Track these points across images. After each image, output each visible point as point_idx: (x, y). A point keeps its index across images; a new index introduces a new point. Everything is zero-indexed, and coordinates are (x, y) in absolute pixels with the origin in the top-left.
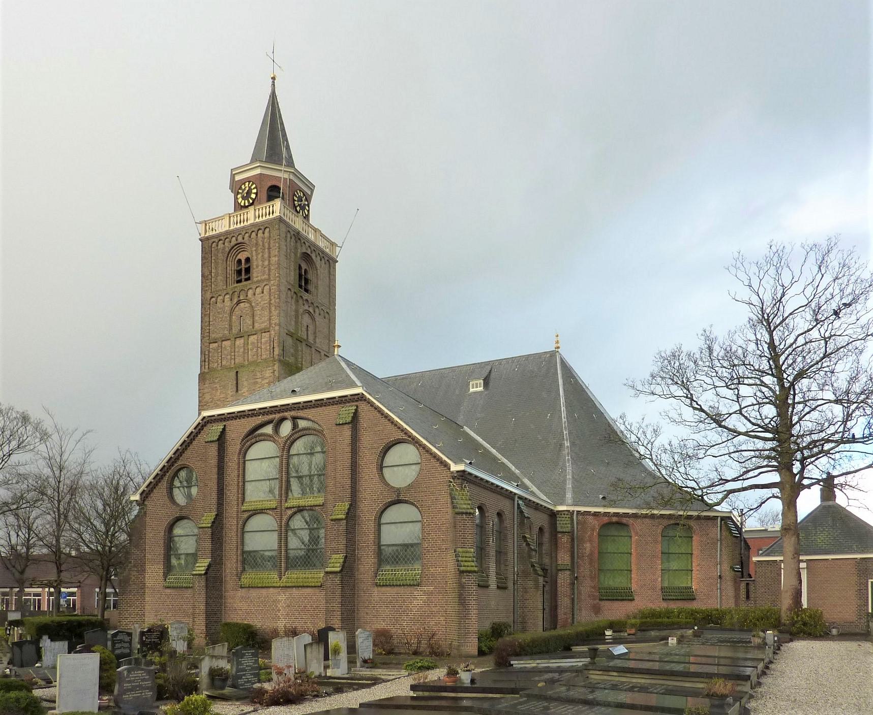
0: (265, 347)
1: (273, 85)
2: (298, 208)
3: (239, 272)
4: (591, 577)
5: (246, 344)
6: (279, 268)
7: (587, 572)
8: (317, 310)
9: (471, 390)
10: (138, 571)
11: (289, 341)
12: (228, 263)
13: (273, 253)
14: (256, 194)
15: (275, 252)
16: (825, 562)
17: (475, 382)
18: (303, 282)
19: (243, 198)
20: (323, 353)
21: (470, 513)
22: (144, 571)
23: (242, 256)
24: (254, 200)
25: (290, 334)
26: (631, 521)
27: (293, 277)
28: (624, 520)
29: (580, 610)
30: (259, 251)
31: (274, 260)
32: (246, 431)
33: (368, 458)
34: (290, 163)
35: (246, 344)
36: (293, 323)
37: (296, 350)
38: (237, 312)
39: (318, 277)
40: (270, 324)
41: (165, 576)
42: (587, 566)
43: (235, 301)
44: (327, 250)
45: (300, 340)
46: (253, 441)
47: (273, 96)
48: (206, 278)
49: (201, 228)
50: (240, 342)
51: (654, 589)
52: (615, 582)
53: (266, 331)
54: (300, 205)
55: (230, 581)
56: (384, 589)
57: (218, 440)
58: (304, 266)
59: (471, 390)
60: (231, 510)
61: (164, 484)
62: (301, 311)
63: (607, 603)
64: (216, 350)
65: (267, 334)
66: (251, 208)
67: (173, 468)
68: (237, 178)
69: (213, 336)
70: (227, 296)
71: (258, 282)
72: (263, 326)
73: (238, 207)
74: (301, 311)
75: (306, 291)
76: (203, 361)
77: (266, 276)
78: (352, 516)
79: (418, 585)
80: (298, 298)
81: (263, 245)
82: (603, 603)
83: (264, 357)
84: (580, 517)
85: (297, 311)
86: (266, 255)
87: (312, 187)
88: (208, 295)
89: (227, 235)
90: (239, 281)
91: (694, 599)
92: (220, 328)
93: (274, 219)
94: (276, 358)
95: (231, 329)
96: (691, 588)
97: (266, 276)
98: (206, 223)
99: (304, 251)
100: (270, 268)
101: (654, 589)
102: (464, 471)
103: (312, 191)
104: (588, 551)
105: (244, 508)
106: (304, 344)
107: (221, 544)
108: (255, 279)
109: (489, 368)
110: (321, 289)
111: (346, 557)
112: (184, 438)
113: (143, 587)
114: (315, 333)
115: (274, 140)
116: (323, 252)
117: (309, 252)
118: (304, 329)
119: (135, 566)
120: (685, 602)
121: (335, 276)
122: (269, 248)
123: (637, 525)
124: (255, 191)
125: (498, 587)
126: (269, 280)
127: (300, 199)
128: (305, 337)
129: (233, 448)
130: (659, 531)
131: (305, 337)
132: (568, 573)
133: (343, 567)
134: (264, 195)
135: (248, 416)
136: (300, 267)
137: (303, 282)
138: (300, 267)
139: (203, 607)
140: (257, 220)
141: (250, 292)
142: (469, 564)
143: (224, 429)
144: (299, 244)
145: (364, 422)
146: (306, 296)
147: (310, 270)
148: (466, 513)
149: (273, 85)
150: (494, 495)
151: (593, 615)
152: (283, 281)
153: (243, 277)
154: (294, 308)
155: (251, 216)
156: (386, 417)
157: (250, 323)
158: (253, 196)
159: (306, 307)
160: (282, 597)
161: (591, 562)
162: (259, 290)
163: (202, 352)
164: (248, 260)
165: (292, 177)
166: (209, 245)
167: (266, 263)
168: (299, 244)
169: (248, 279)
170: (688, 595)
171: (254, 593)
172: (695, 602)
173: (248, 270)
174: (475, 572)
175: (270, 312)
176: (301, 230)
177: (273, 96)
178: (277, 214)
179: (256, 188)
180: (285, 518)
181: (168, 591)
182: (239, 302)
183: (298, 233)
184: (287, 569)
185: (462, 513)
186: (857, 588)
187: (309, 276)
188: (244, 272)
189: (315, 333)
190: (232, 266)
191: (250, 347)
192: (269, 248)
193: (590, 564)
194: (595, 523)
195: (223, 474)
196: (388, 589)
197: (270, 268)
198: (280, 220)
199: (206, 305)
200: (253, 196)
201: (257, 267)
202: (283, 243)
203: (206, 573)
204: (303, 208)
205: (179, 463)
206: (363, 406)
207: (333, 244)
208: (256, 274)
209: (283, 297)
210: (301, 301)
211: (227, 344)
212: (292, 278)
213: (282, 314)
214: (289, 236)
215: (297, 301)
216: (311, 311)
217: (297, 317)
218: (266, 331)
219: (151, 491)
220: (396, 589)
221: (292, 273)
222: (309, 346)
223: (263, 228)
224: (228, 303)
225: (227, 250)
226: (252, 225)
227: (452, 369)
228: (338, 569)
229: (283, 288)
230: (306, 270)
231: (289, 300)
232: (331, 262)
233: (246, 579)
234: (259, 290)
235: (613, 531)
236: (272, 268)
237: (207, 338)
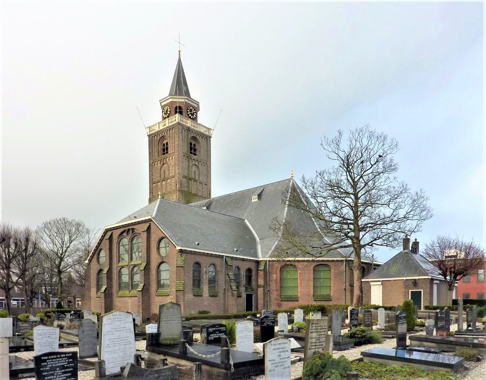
0: (174, 184)
2: (190, 115)
3: (164, 150)
6: (178, 147)
7: (274, 288)
8: (200, 163)
9: (253, 201)
12: (159, 145)
15: (177, 139)
18: (193, 150)
20: (203, 183)
22: (90, 291)
23: (165, 142)
24: (169, 114)
25: (185, 177)
26: (296, 264)
27: (186, 149)
29: (271, 305)
31: (176, 143)
32: (119, 233)
34: (187, 93)
36: (186, 171)
38: (163, 169)
41: (97, 292)
43: (162, 163)
47: (180, 61)
48: (150, 153)
49: (148, 130)
50: (164, 183)
51: (309, 295)
52: (289, 293)
54: (191, 114)
55: (115, 294)
58: (193, 143)
59: (253, 201)
61: (95, 256)
64: (155, 187)
66: (167, 119)
68: (163, 104)
69: (154, 180)
71: (171, 154)
73: (164, 118)
76: (150, 193)
78: (147, 269)
80: (189, 158)
82: (282, 302)
84: (271, 263)
85: (188, 165)
87: (198, 103)
88: (152, 162)
89: (158, 133)
90: (164, 154)
95: (161, 177)
98: (150, 127)
99: (192, 135)
100: (181, 144)
101: (309, 295)
102: (181, 249)
103: (198, 105)
104: (275, 278)
107: (112, 280)
108: (169, 153)
110: (202, 152)
112: (100, 238)
113: (90, 297)
115: (180, 84)
116: (203, 134)
117: (195, 136)
118: (193, 173)
120: (326, 302)
121: (210, 144)
126: (174, 153)
127: (191, 110)
128: (194, 177)
129: (115, 241)
130: (312, 268)
131: (194, 177)
132: (262, 288)
133: (143, 289)
134: (173, 112)
135: (119, 228)
136: (191, 144)
137: (193, 150)
138: (191, 144)
141: (168, 159)
143: (112, 234)
146: (194, 157)
147: (196, 145)
153: (166, 152)
155: (168, 123)
158: (169, 112)
159: (194, 163)
160: (130, 300)
161: (276, 283)
162: (171, 158)
163: (150, 189)
164: (167, 143)
165: (186, 101)
166: (151, 137)
169: (167, 153)
173: (167, 149)
176: (190, 126)
177: (180, 61)
178: (177, 121)
180: (131, 269)
182: (163, 164)
183: (189, 128)
184: (132, 289)
186: (404, 294)
187: (197, 147)
188: (165, 150)
190: (161, 147)
194: (278, 266)
197: (181, 144)
198: (179, 123)
199: (151, 166)
200: (169, 112)
202: (180, 134)
204: (193, 115)
206: (152, 223)
207: (209, 129)
209: (181, 160)
210: (191, 160)
211: (159, 184)
212: (186, 150)
214: (183, 130)
215: (189, 160)
216: (197, 163)
217: (188, 168)
219: (92, 259)
221: (186, 148)
222: (195, 181)
224: (159, 165)
226: (168, 127)
227: (229, 195)
229: (180, 156)
230: (194, 145)
231: (184, 161)
232: (208, 138)
233: (121, 293)
234: (171, 158)
235: (321, 268)
236: (177, 146)
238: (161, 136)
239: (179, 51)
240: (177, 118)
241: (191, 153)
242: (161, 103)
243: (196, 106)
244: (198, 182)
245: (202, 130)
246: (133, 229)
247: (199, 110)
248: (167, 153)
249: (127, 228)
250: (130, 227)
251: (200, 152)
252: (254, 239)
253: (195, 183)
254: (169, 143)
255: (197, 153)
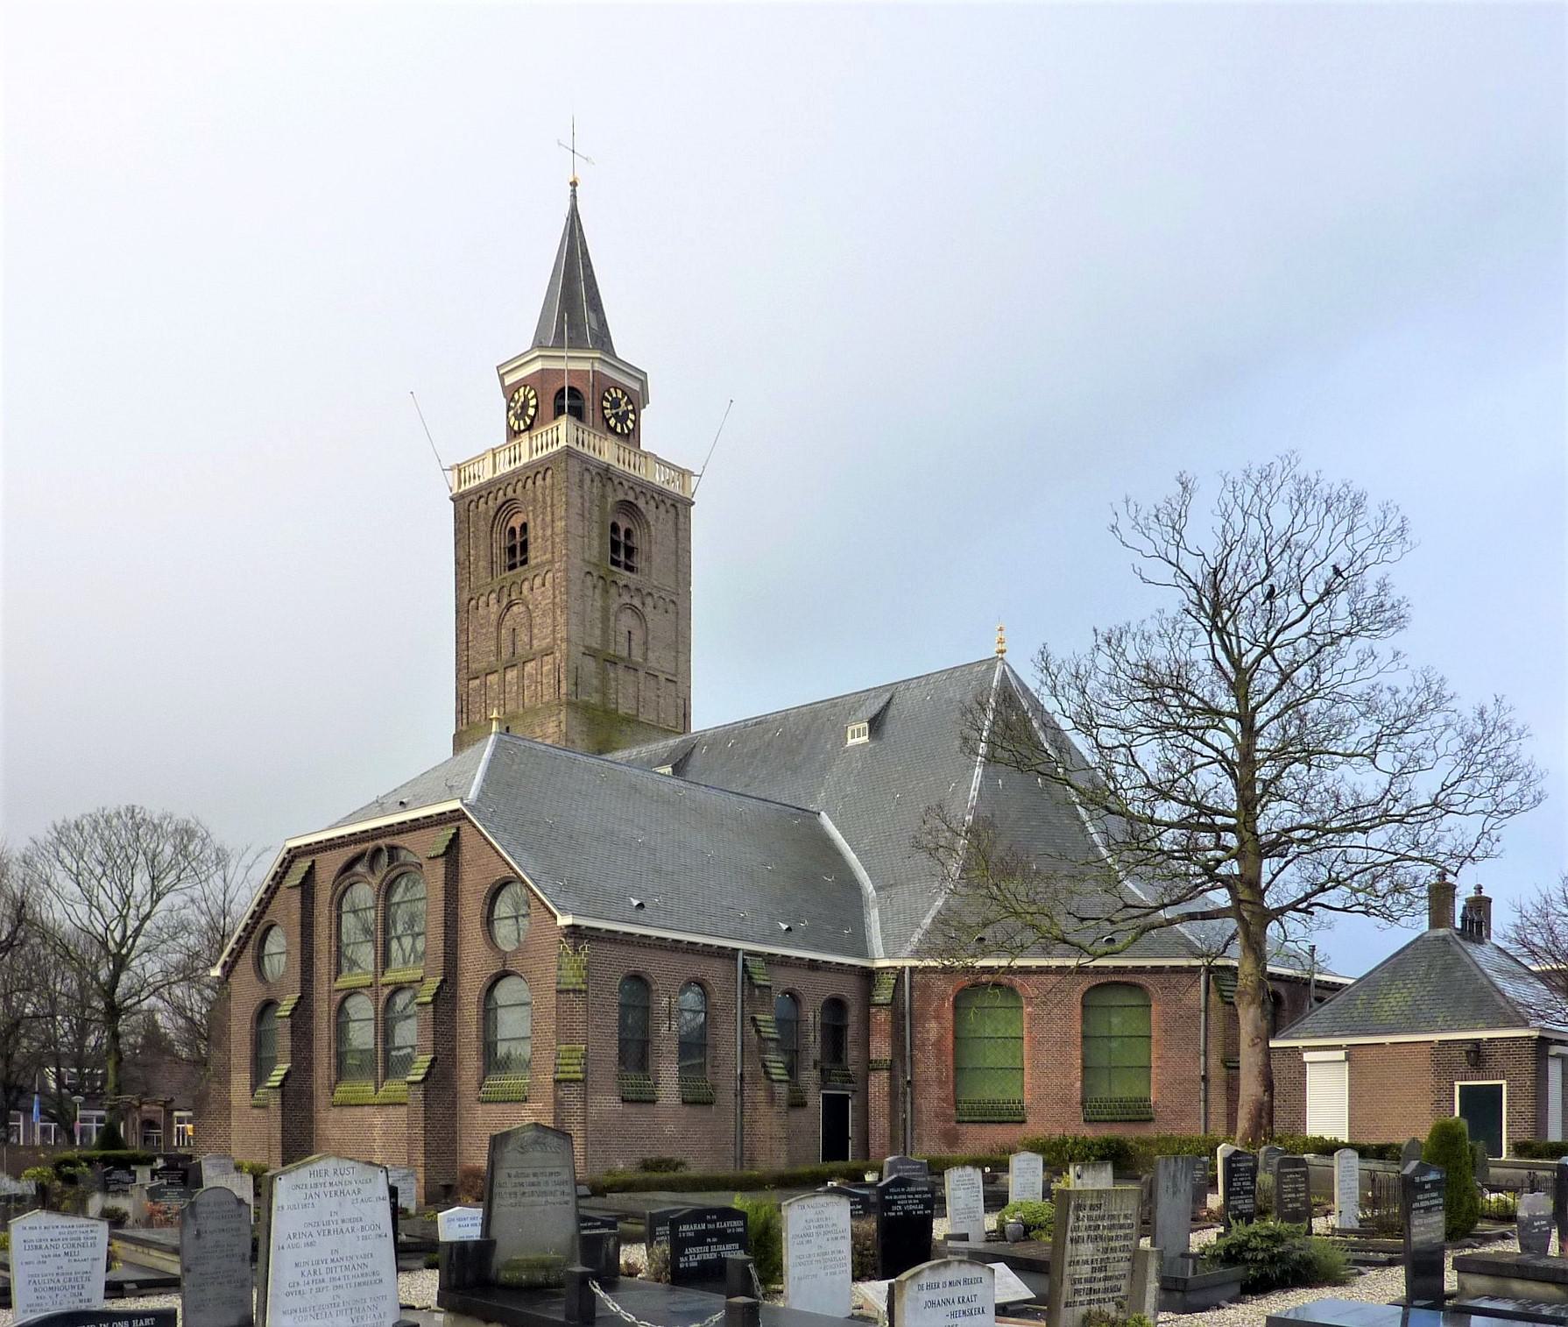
0: (549, 680)
1: (574, 196)
2: (612, 422)
3: (512, 550)
4: (940, 1082)
5: (521, 677)
6: (566, 540)
7: (932, 1073)
8: (649, 601)
9: (851, 742)
10: (219, 1083)
11: (590, 665)
12: (494, 532)
13: (557, 512)
14: (536, 407)
16: (1374, 1051)
17: (856, 727)
19: (517, 417)
20: (662, 677)
21: (580, 991)
22: (229, 1082)
23: (516, 522)
24: (532, 419)
25: (590, 653)
26: (1017, 980)
27: (597, 547)
28: (1004, 980)
30: (539, 511)
31: (560, 524)
33: (471, 909)
34: (603, 340)
35: (521, 677)
36: (598, 632)
37: (604, 681)
39: (652, 540)
40: (554, 639)
42: (933, 1060)
43: (505, 602)
44: (671, 488)
45: (613, 661)
46: (347, 883)
49: (452, 477)
50: (511, 675)
51: (1065, 1101)
52: (989, 1091)
53: (548, 652)
54: (616, 415)
56: (488, 1106)
57: (302, 884)
58: (623, 524)
59: (851, 742)
60: (322, 989)
61: (249, 952)
62: (614, 607)
63: (973, 1129)
65: (549, 659)
67: (259, 926)
68: (509, 380)
70: (493, 596)
71: (537, 566)
72: (544, 643)
73: (513, 434)
74: (614, 607)
75: (630, 568)
76: (459, 712)
77: (548, 556)
78: (446, 997)
79: (526, 1100)
80: (607, 583)
81: (544, 502)
82: (964, 1128)
83: (546, 698)
84: (917, 977)
85: (605, 610)
86: (548, 519)
88: (466, 596)
90: (512, 567)
91: (1151, 1120)
92: (484, 654)
93: (558, 452)
94: (563, 698)
95: (499, 652)
96: (1147, 1100)
97: (548, 556)
98: (459, 468)
99: (621, 497)
100: (577, 535)
102: (573, 926)
104: (933, 1036)
105: (337, 986)
106: (621, 666)
108: (532, 562)
109: (888, 696)
111: (434, 1060)
113: (228, 1106)
114: (646, 643)
115: (575, 301)
116: (661, 492)
117: (631, 498)
118: (622, 640)
119: (215, 1075)
122: (552, 505)
123: (1028, 987)
124: (533, 402)
125: (684, 1102)
126: (552, 562)
127: (616, 403)
129: (324, 894)
131: (625, 654)
133: (428, 1074)
134: (548, 408)
136: (615, 528)
138: (615, 528)
139: (279, 1136)
140: (535, 457)
141: (526, 586)
142: (571, 1068)
143: (312, 867)
144: (609, 489)
145: (467, 853)
146: (624, 576)
147: (635, 533)
148: (574, 991)
149: (574, 196)
150: (676, 955)
151: (944, 1148)
152: (578, 562)
153: (518, 558)
154: (598, 604)
155: (527, 451)
156: (490, 844)
157: (526, 639)
158: (531, 412)
159: (626, 599)
160: (378, 1119)
162: (538, 581)
163: (459, 697)
164: (524, 527)
165: (597, 366)
166: (465, 504)
167: (549, 532)
168: (609, 489)
169: (524, 562)
170: (1140, 1113)
171: (347, 1112)
172: (1152, 1126)
173: (524, 545)
174: (577, 1080)
175: (554, 619)
178: (563, 443)
179: (535, 396)
181: (256, 1111)
182: (509, 606)
184: (386, 1076)
185: (568, 991)
187: (638, 541)
188: (518, 552)
189: (646, 643)
191: (526, 682)
192: (552, 505)
193: (938, 1057)
195: (311, 935)
196: (494, 1106)
197: (577, 535)
198: (568, 452)
199: (464, 611)
200: (531, 412)
201: (536, 539)
202: (575, 494)
203: (282, 1085)
204: (622, 419)
205: (266, 918)
207: (684, 473)
208: (535, 555)
209: (575, 589)
210: (613, 590)
211: (493, 678)
212: (595, 552)
213: (574, 620)
214: (587, 477)
215: (606, 591)
216: (636, 602)
217: (605, 619)
218: (548, 652)
219: (235, 962)
220: (501, 1106)
221: (596, 543)
222: (632, 668)
223: (542, 470)
224: (494, 608)
225: (492, 513)
226: (526, 467)
227: (760, 722)
228: (420, 1078)
229: (575, 575)
230: (628, 533)
231: (589, 592)
232: (679, 507)
233: (344, 1090)
234: (538, 581)
236: (561, 537)
237: (466, 672)
238: (500, 500)
239: (574, 184)
240: (561, 432)
241: (615, 562)
242: (502, 377)
243: (636, 386)
244: (641, 674)
245: (658, 478)
246: (393, 849)
247: (646, 401)
248: (524, 562)
249: (370, 845)
250: (381, 842)
251: (649, 559)
252: (856, 887)
253: (630, 677)
254: (531, 525)
255: (638, 561)
